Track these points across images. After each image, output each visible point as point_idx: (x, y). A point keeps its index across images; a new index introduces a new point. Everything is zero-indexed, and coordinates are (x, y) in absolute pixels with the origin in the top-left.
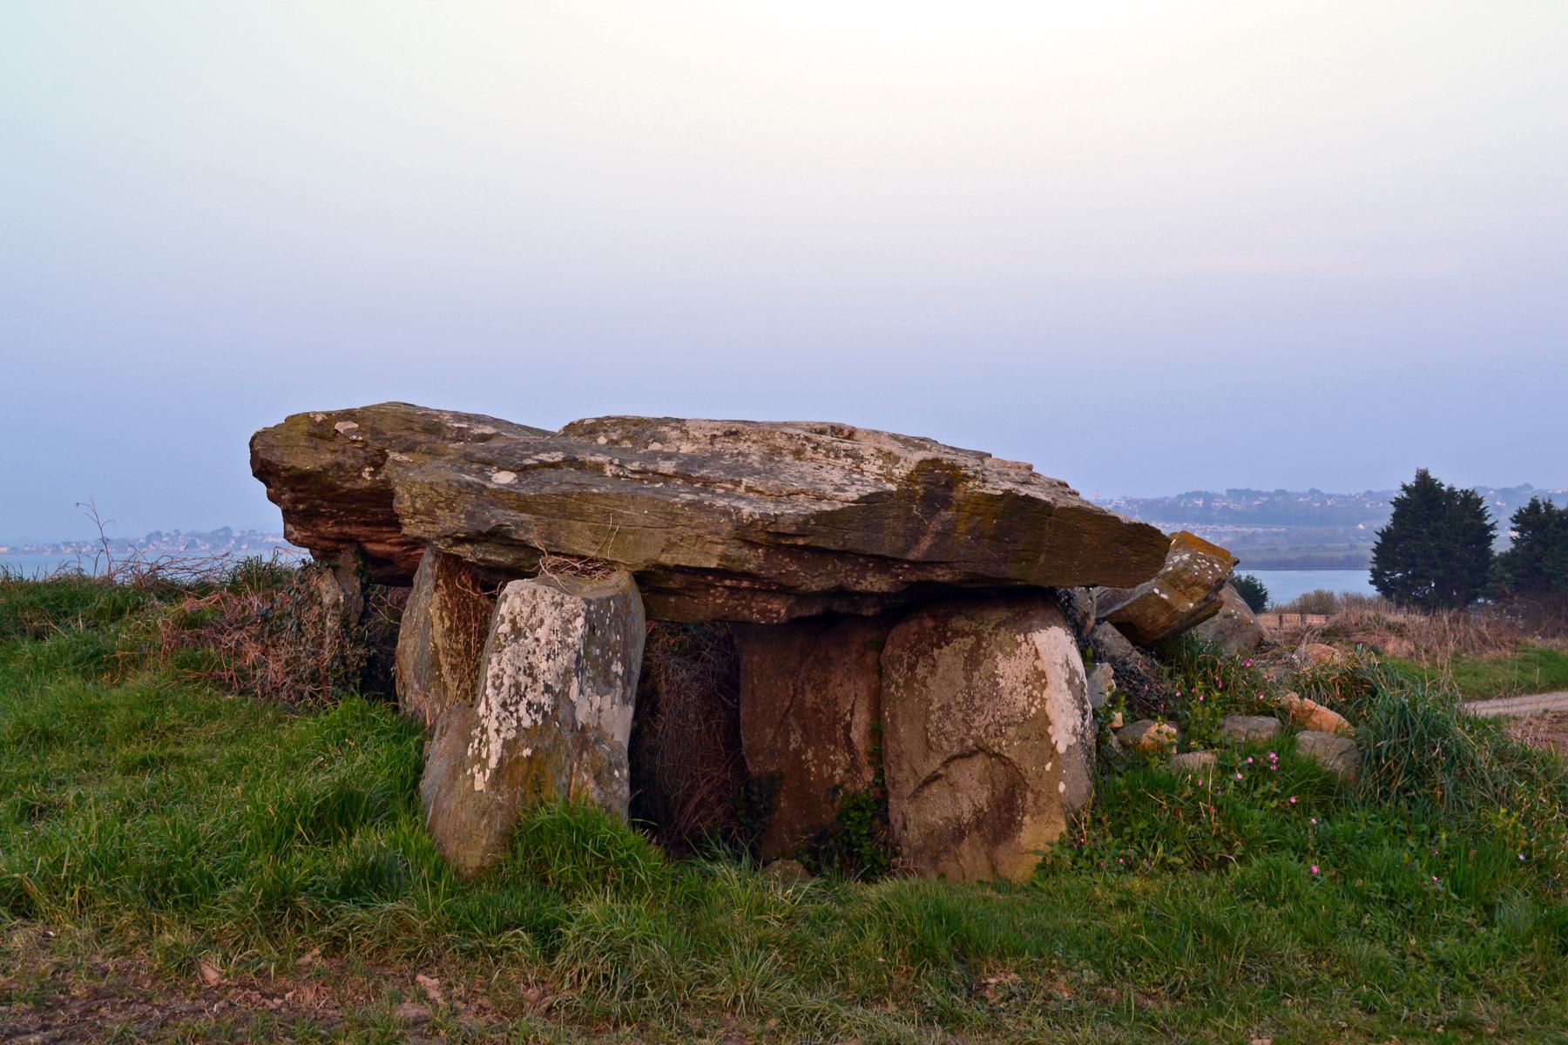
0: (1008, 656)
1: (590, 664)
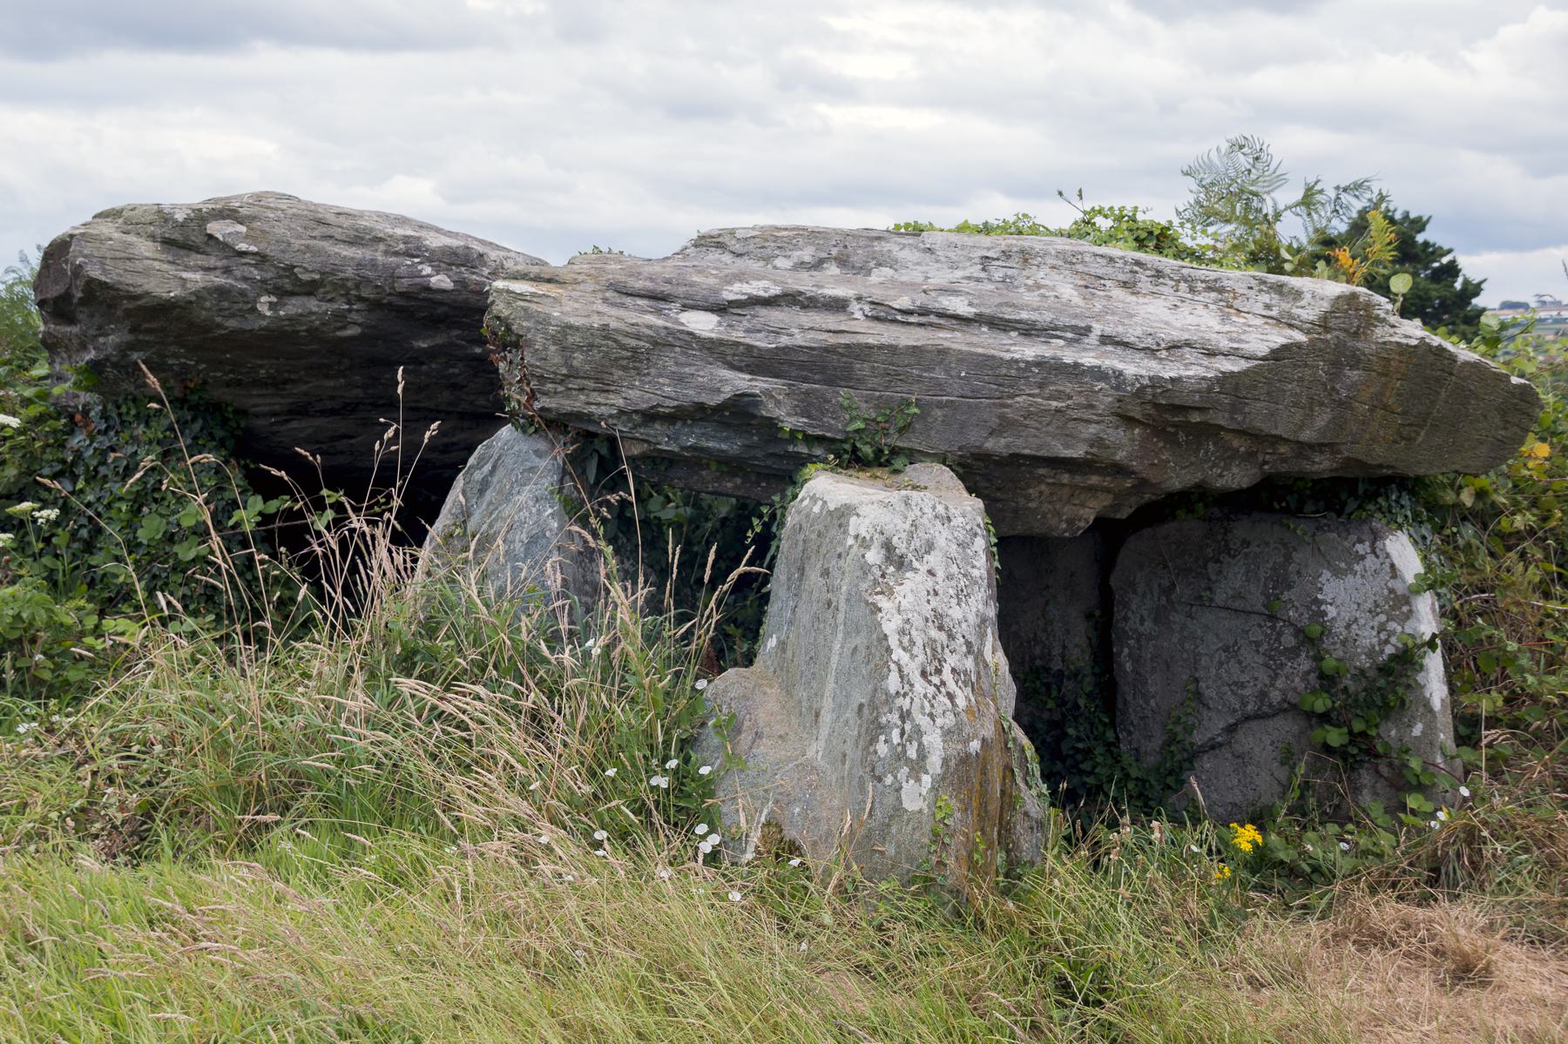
0: (1338, 573)
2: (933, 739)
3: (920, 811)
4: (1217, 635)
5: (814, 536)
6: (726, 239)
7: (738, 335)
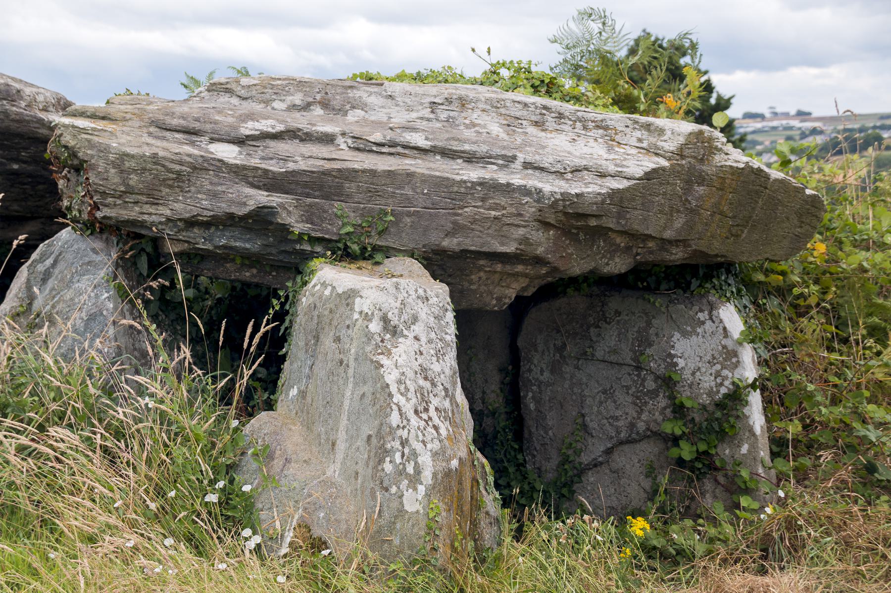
0: (685, 334)
2: (425, 459)
3: (417, 512)
4: (598, 382)
5: (326, 313)
6: (233, 86)
7: (255, 162)
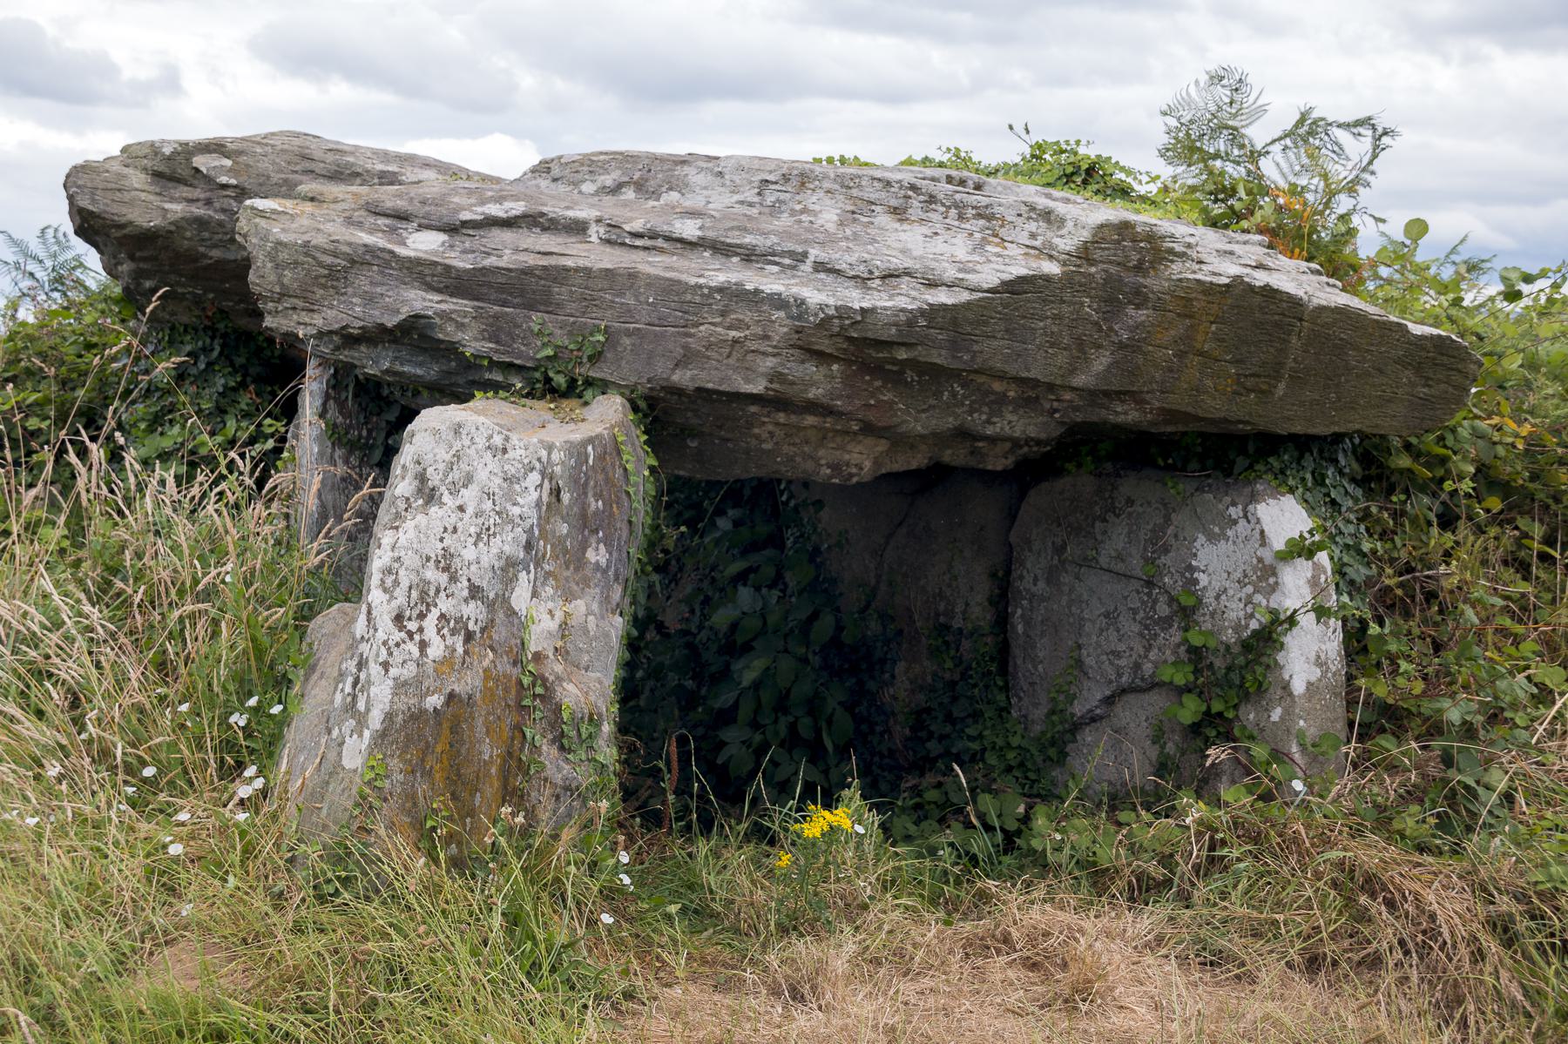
0: (1212, 538)
1: (550, 553)
3: (355, 771)
